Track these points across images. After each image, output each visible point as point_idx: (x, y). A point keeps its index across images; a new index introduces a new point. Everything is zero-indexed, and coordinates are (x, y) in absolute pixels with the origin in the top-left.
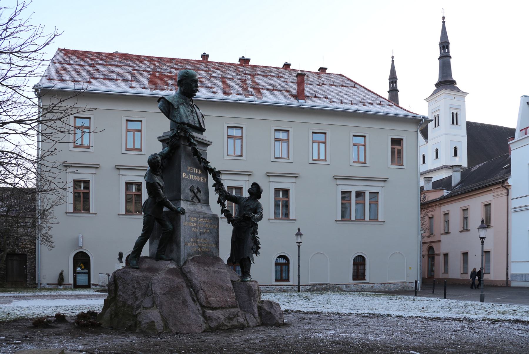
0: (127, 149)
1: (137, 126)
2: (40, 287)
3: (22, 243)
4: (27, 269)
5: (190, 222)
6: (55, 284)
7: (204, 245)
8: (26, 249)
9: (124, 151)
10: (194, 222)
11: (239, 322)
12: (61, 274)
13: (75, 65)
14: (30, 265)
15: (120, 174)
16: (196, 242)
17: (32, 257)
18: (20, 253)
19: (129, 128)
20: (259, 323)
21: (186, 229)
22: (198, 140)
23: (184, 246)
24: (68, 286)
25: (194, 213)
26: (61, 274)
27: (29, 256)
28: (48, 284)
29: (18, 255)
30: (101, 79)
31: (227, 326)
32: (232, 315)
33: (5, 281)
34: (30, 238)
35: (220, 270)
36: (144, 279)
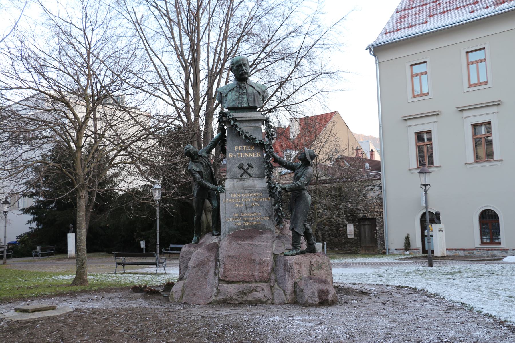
0: (414, 96)
1: (479, 56)
2: (389, 253)
3: (371, 206)
4: (377, 234)
5: (231, 198)
6: (401, 249)
7: (252, 219)
8: (375, 213)
9: (410, 99)
10: (237, 198)
11: (255, 298)
12: (407, 238)
13: (418, 6)
14: (380, 229)
15: (464, 116)
16: (241, 217)
17: (380, 220)
18: (370, 217)
19: (470, 60)
20: (288, 300)
21: (227, 206)
22: (239, 119)
23: (225, 222)
24: (415, 251)
25: (238, 189)
26: (407, 238)
27: (378, 220)
28: (396, 249)
29: (369, 219)
30: (441, 13)
31: (237, 300)
32: (247, 290)
33: (359, 247)
34: (378, 200)
35: (259, 243)
36: (188, 253)
